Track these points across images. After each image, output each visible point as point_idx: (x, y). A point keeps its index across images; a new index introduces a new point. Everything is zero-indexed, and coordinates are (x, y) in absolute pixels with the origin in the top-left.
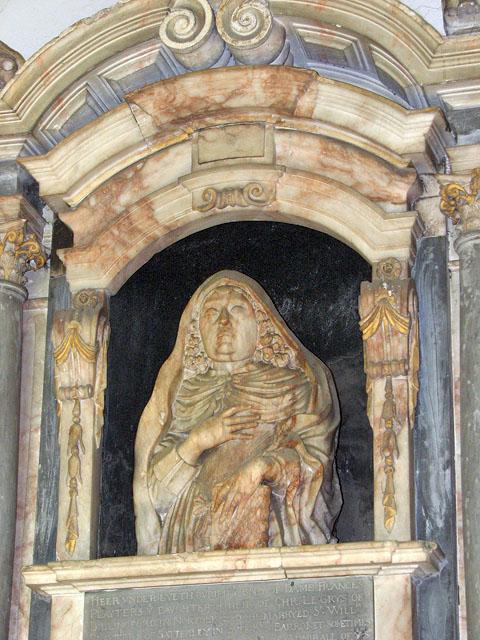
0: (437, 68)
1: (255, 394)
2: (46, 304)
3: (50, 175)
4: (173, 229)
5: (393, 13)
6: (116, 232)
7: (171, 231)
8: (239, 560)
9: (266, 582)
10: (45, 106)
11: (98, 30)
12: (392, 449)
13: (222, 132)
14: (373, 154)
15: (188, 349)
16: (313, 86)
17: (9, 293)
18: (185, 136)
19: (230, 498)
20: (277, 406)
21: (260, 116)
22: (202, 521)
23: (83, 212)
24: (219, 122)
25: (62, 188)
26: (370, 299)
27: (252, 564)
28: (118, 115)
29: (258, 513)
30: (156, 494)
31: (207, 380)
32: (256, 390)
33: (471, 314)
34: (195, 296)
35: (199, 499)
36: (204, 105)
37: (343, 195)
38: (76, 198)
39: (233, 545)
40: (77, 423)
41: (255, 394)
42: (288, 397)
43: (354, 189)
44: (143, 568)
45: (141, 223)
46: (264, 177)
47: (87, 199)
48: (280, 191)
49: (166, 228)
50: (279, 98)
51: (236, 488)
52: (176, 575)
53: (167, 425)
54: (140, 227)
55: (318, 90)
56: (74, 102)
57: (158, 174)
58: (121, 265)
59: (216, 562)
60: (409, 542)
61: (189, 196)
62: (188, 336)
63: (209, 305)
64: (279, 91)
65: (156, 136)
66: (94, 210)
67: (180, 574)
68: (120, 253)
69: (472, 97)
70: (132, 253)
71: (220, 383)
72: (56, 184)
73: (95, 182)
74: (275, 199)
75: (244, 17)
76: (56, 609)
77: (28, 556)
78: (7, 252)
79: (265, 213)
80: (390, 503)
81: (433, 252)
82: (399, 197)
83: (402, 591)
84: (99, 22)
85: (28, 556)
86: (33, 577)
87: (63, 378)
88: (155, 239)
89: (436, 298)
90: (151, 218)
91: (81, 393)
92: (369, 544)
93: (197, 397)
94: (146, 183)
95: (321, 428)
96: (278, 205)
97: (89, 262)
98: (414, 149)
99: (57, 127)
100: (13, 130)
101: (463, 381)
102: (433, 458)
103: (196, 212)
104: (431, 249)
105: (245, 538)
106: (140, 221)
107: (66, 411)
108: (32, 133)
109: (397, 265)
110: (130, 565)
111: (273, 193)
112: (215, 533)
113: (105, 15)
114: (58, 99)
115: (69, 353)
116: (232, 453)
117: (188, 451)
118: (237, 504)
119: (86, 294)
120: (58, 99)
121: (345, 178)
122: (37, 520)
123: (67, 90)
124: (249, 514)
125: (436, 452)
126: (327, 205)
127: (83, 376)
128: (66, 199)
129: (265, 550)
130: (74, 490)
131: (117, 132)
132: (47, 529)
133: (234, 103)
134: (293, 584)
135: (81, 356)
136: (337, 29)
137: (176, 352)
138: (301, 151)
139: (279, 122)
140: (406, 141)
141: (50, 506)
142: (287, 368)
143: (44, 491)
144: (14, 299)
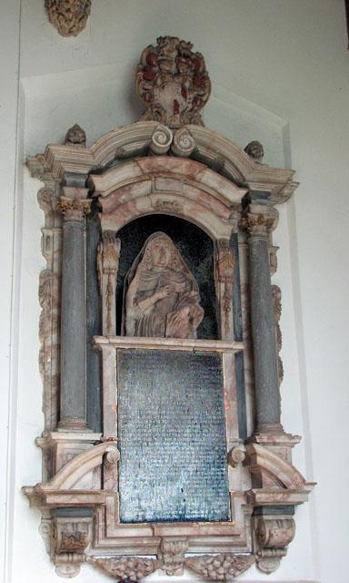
3: (101, 183)
13: (164, 180)
14: (221, 199)
23: (108, 200)
27: (184, 344)
37: (208, 213)
39: (176, 336)
45: (132, 209)
46: (180, 200)
47: (109, 195)
59: (171, 342)
66: (112, 200)
68: (122, 218)
76: (104, 353)
80: (227, 329)
107: (104, 279)
117: (153, 299)
120: (267, 182)
123: (270, 183)
126: (202, 215)
130: (109, 309)
133: (175, 171)
138: (192, 193)
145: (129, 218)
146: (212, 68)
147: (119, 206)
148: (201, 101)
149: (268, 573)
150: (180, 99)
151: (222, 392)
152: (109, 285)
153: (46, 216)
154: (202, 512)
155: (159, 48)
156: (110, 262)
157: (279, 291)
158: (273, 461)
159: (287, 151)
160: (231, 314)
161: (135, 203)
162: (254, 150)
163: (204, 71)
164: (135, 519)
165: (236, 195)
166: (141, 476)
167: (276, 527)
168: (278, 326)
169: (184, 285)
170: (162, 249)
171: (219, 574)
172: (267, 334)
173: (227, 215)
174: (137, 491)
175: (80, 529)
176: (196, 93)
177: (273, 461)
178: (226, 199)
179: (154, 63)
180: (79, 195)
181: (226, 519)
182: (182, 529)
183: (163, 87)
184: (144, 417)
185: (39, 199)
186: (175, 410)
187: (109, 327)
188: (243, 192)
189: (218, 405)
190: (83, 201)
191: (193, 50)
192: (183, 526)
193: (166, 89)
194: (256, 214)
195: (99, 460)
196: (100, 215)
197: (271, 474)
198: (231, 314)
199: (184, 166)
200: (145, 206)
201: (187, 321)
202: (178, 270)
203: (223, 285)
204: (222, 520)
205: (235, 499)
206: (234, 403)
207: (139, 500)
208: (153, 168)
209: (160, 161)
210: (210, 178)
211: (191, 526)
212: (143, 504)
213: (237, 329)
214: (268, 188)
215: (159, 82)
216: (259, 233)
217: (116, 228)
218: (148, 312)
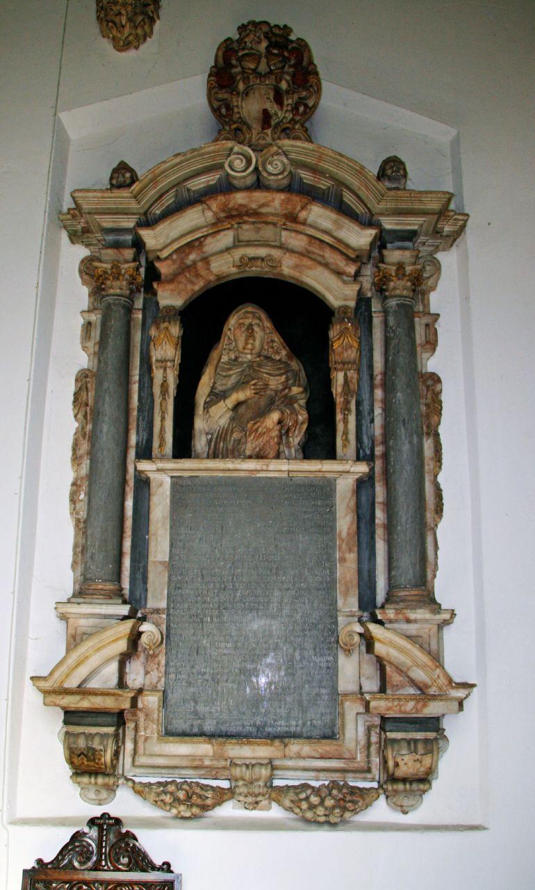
0: (382, 206)
1: (266, 373)
2: (141, 312)
3: (151, 238)
4: (221, 276)
5: (360, 172)
6: (188, 276)
7: (219, 278)
9: (276, 478)
10: (154, 199)
11: (188, 160)
12: (346, 409)
13: (252, 226)
14: (340, 247)
15: (226, 345)
16: (308, 207)
17: (125, 303)
18: (229, 226)
19: (260, 430)
21: (275, 219)
22: (239, 441)
23: (169, 262)
24: (250, 220)
25: (159, 247)
26: (338, 327)
27: (271, 467)
28: (195, 209)
29: (276, 440)
31: (236, 363)
32: (267, 371)
33: (395, 341)
34: (232, 316)
36: (245, 210)
37: (320, 269)
38: (164, 254)
39: (259, 456)
40: (165, 381)
41: (266, 373)
42: (284, 377)
43: (326, 265)
44: (208, 465)
45: (203, 272)
46: (276, 253)
47: (171, 255)
48: (284, 262)
49: (217, 276)
50: (290, 210)
51: (264, 425)
52: (226, 470)
53: (213, 388)
55: (311, 209)
56: (169, 200)
57: (212, 245)
58: (190, 294)
59: (251, 465)
61: (231, 259)
62: (226, 338)
63: (241, 321)
64: (289, 207)
65: (214, 224)
66: (174, 262)
67: (229, 470)
68: (189, 287)
69: (397, 224)
70: (197, 288)
71: (245, 365)
72: (156, 245)
73: (176, 246)
74: (281, 266)
75: (275, 162)
76: (153, 485)
77: (132, 454)
79: (274, 274)
81: (365, 305)
83: (351, 487)
84: (188, 156)
85: (132, 454)
86: (142, 466)
87: (156, 354)
88: (210, 281)
89: (366, 330)
90: (208, 269)
91: (169, 364)
92: (150, 461)
93: (231, 372)
94: (205, 249)
95: (303, 395)
96: (281, 270)
98: (364, 248)
99: (158, 212)
100: (135, 211)
101: (385, 374)
102: (364, 417)
103: (234, 269)
104: (364, 303)
107: (158, 375)
108: (145, 213)
109: (349, 310)
111: (280, 262)
112: (249, 448)
113: (193, 152)
114: (161, 196)
117: (231, 402)
118: (264, 433)
119: (169, 309)
120: (161, 196)
121: (320, 259)
122: (137, 434)
125: (366, 414)
126: (310, 272)
127: (169, 354)
128: (159, 253)
129: (277, 461)
130: (163, 419)
131: (193, 218)
133: (264, 210)
134: (291, 480)
136: (326, 177)
138: (297, 242)
139: (284, 224)
140: (359, 243)
142: (280, 360)
145: (199, 286)
146: (319, 56)
148: (306, 106)
149: (405, 813)
150: (272, 108)
151: (333, 540)
152: (164, 386)
153: (90, 295)
154: (294, 723)
155: (240, 41)
156: (167, 350)
157: (439, 381)
158: (401, 650)
159: (457, 172)
162: (392, 169)
163: (311, 63)
164: (188, 731)
165: (360, 238)
166: (201, 667)
167: (404, 752)
168: (437, 435)
170: (251, 326)
172: (406, 448)
173: (351, 269)
174: (191, 690)
175: (96, 744)
176: (296, 96)
177: (401, 650)
178: (347, 246)
179: (234, 62)
180: (121, 259)
181: (330, 735)
182: (257, 748)
183: (247, 94)
184: (207, 579)
185: (80, 272)
186: (256, 568)
188: (371, 233)
189: (327, 558)
190: (126, 266)
191: (293, 37)
192: (259, 745)
193: (251, 95)
194: (393, 264)
195: (122, 646)
197: (400, 670)
199: (277, 203)
200: (224, 266)
201: (275, 433)
202: (278, 357)
204: (325, 737)
205: (347, 704)
206: (352, 557)
207: (196, 702)
208: (231, 210)
209: (240, 198)
210: (319, 215)
211: (271, 745)
212: (201, 708)
214: (412, 223)
215: (241, 87)
216: (398, 292)
217: (178, 302)
218: (224, 422)
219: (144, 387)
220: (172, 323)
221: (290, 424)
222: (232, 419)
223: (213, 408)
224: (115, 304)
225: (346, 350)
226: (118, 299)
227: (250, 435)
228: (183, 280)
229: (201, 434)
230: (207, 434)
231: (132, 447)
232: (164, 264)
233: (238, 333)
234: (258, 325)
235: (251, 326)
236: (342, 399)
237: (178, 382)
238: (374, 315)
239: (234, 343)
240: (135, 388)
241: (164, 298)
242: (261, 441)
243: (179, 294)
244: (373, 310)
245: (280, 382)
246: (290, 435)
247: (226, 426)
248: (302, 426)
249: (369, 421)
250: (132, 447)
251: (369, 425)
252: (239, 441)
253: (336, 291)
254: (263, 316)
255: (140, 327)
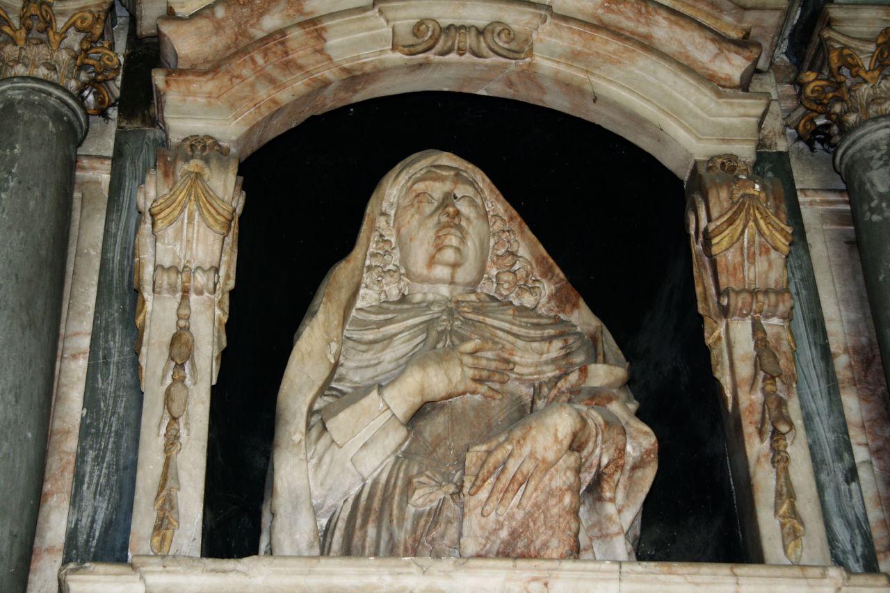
2: (109, 162)
6: (260, 60)
7: (354, 78)
8: (535, 579)
17: (65, 110)
19: (512, 466)
20: (541, 354)
23: (205, 25)
26: (724, 194)
30: (320, 475)
31: (405, 306)
35: (423, 479)
49: (344, 70)
51: (526, 450)
54: (301, 61)
60: (819, 578)
61: (388, 31)
63: (420, 187)
66: (219, 27)
70: (285, 97)
71: (436, 309)
78: (66, 48)
81: (772, 169)
82: (728, 79)
90: (321, 51)
97: (210, 96)
104: (768, 166)
105: (538, 543)
106: (301, 53)
110: (310, 573)
115: (182, 210)
116: (472, 414)
117: (402, 398)
118: (527, 479)
124: (546, 501)
127: (201, 255)
130: (172, 441)
132: (93, 521)
135: (201, 214)
137: (358, 252)
141: (102, 480)
143: (91, 454)
144: (70, 123)
145: (293, 88)
147: (241, 49)
152: (180, 345)
160: (797, 451)
161: (320, 36)
169: (555, 350)
171: (618, 461)
187: (162, 525)
196: (159, 78)
198: (797, 451)
201: (562, 478)
203: (742, 332)
213: (842, 534)
219: (107, 364)
220: (214, 163)
221: (605, 461)
222: (404, 456)
223: (342, 416)
224: (29, 105)
225: (752, 258)
226: (41, 91)
227: (476, 488)
228: (246, 72)
229: (295, 508)
230: (315, 511)
231: (50, 550)
232: (187, 28)
233: (411, 221)
234: (472, 202)
235: (448, 199)
236: (758, 397)
237: (224, 344)
238: (801, 198)
239: (397, 254)
240: (74, 372)
241: (185, 115)
242: (515, 507)
243: (232, 106)
244: (797, 187)
245: (545, 357)
246: (608, 494)
247: (384, 477)
248: (639, 473)
249: (841, 478)
250: (50, 550)
251: (844, 487)
252: (436, 514)
253: (696, 116)
254: (480, 177)
255: (103, 206)
